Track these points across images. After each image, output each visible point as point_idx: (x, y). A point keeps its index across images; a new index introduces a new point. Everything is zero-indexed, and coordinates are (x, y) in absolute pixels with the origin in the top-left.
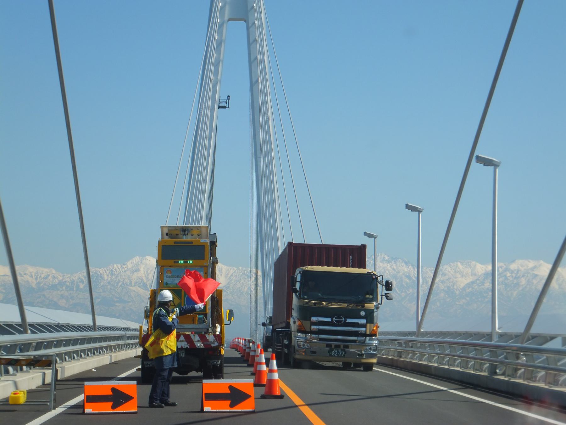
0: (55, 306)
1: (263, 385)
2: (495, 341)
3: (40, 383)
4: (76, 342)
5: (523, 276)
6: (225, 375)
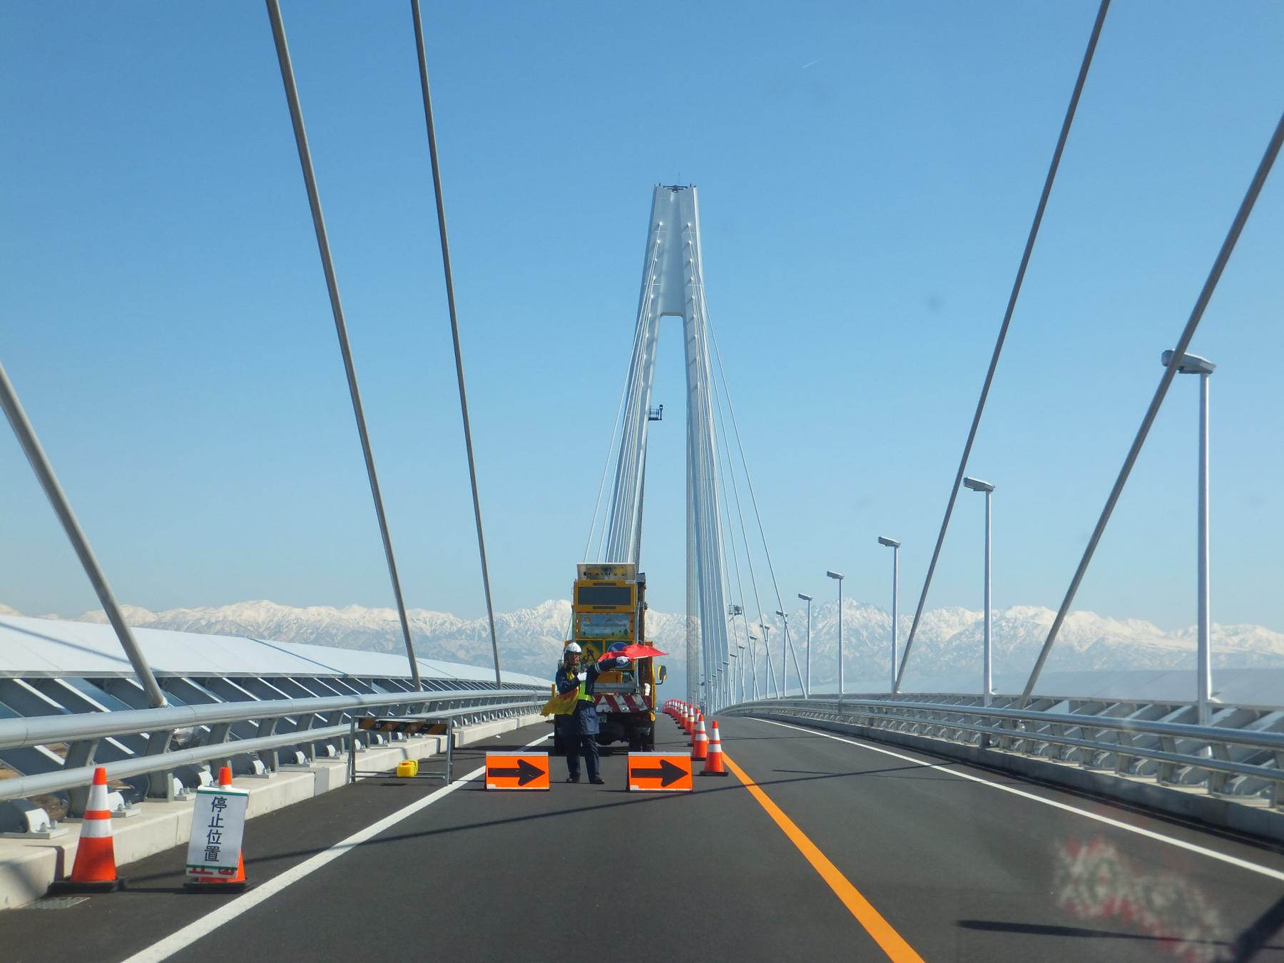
0: (453, 658)
1: (703, 759)
2: (987, 707)
3: (434, 752)
4: (476, 702)
5: (1022, 626)
6: (656, 746)
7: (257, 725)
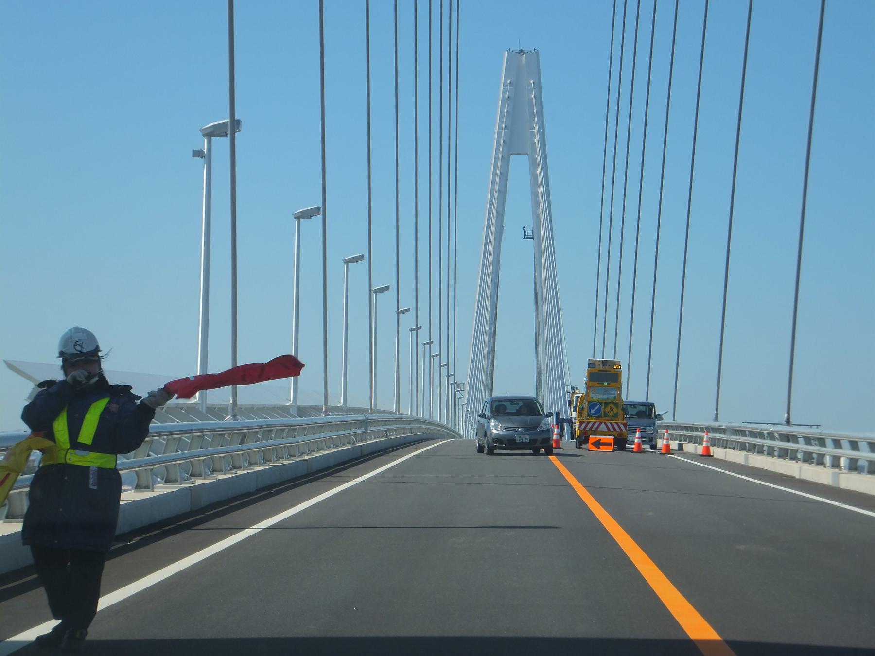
7: (211, 440)
